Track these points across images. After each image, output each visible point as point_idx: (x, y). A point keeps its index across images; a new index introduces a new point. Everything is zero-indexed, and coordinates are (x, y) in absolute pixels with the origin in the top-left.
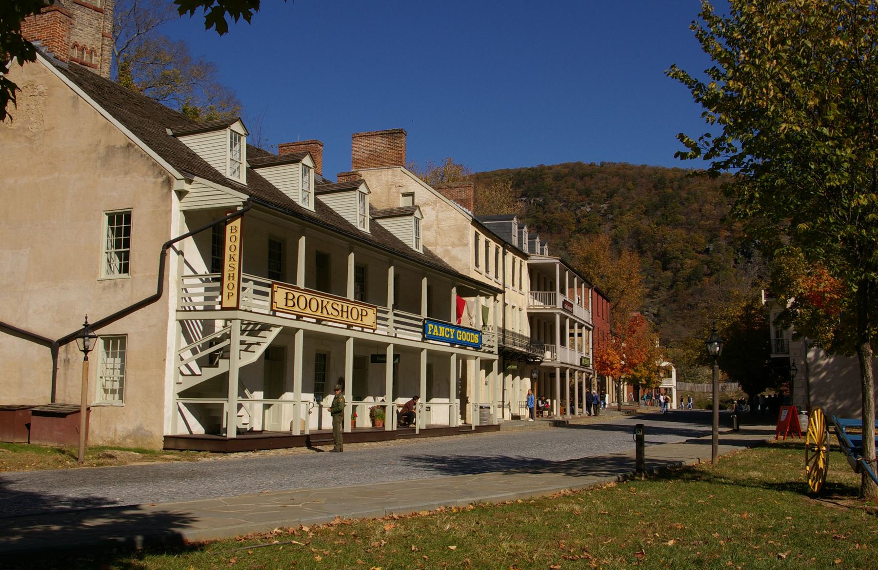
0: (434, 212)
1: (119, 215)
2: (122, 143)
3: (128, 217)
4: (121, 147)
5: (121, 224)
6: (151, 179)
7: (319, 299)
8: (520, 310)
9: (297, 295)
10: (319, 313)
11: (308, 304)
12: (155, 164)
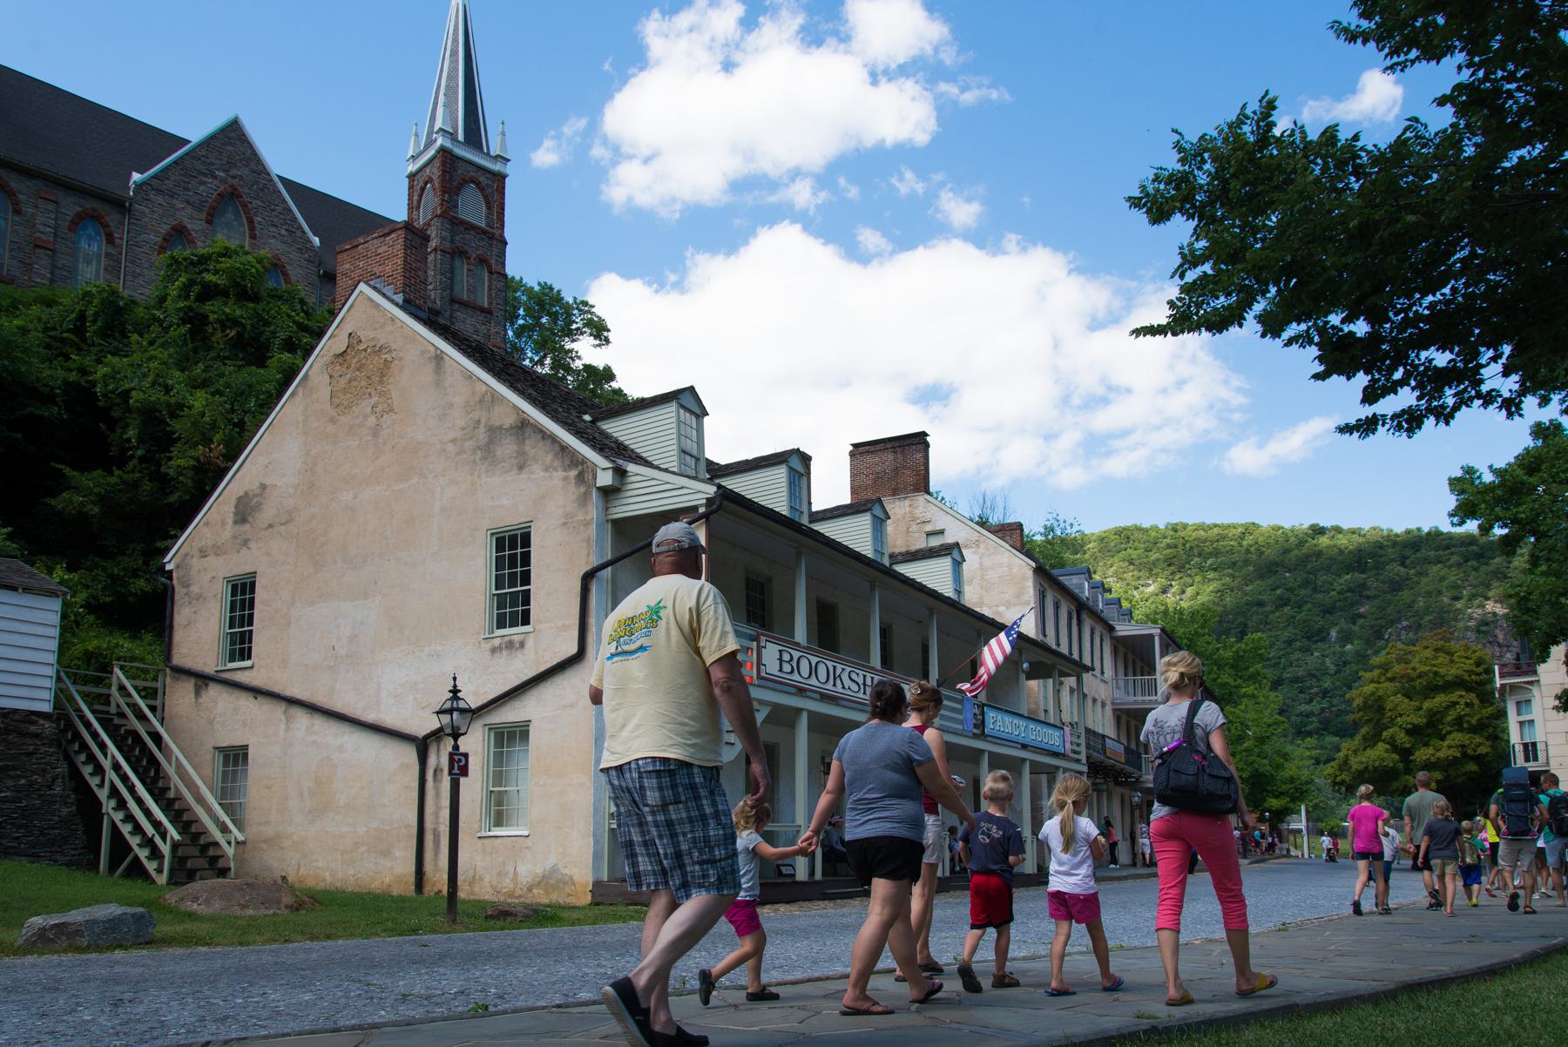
0: (977, 557)
1: (513, 539)
2: (509, 420)
3: (526, 539)
4: (512, 427)
5: (513, 553)
6: (560, 474)
7: (830, 664)
8: (1103, 705)
9: (796, 655)
10: (830, 686)
11: (813, 670)
12: (564, 449)
